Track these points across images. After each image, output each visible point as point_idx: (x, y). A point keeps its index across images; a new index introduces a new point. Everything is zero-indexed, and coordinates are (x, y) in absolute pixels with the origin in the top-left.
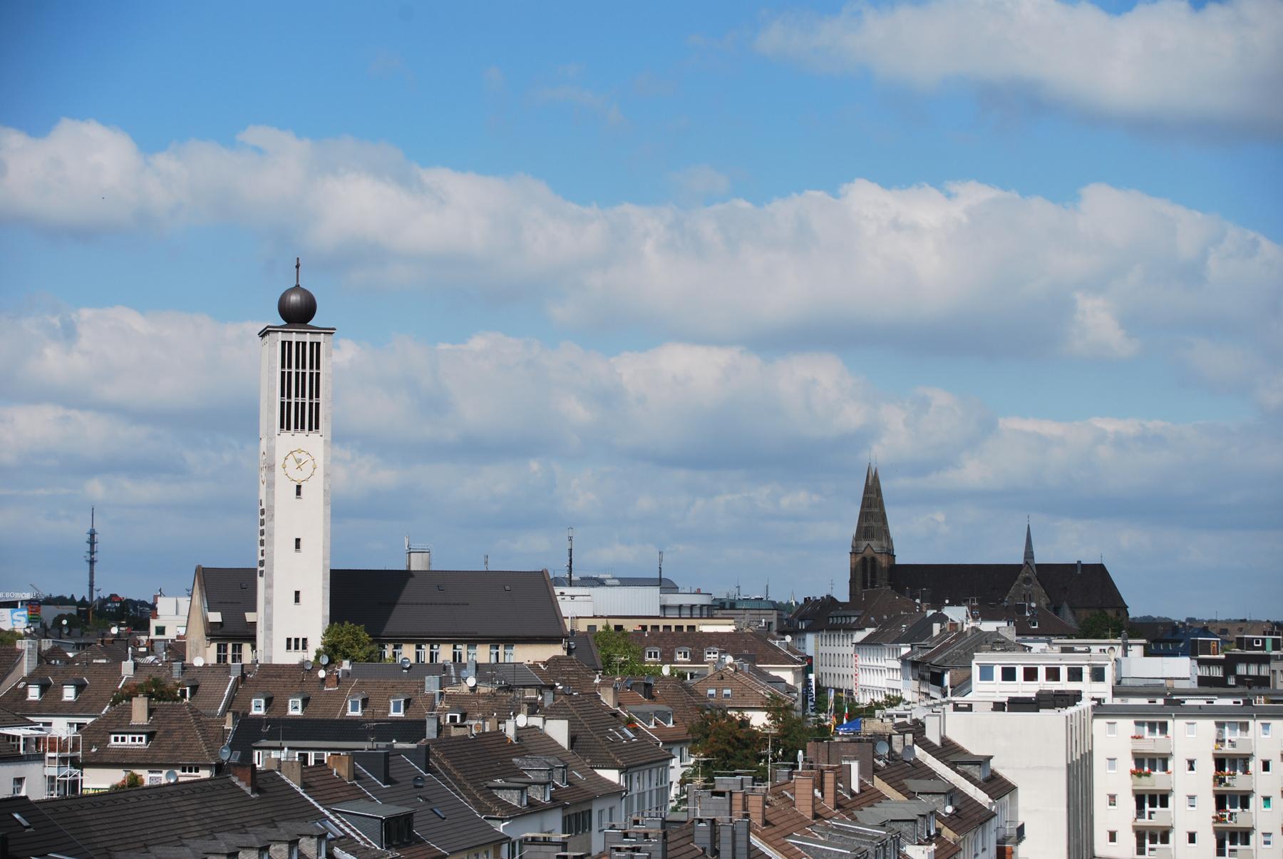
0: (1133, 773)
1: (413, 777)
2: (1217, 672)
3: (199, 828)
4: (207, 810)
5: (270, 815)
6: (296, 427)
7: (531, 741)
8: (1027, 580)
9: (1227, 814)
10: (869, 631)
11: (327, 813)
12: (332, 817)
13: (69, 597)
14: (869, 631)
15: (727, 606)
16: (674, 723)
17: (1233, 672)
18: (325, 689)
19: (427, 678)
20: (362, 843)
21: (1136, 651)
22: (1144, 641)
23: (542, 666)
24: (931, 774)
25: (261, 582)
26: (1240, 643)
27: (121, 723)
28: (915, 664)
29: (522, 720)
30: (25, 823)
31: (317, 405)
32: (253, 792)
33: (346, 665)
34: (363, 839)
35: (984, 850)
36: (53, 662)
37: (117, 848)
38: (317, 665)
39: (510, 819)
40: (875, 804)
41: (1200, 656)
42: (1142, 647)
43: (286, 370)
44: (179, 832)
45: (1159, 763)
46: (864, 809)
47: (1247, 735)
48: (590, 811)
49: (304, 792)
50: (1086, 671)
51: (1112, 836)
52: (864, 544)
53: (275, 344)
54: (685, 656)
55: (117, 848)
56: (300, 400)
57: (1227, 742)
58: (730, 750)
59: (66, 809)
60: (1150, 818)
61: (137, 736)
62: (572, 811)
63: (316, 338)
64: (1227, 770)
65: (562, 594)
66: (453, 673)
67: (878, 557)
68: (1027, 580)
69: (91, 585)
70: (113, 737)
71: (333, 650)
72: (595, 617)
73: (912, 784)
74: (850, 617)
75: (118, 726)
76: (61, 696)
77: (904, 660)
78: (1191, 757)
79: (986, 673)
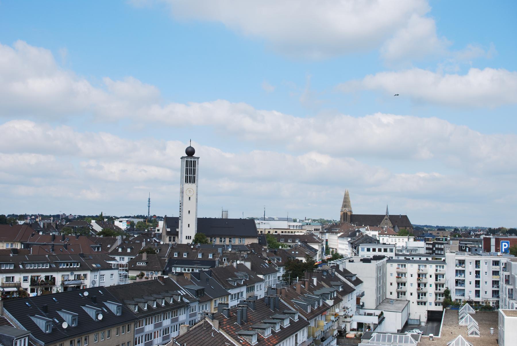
0: (397, 277)
1: (206, 278)
2: (431, 246)
3: (147, 293)
4: (150, 288)
5: (167, 289)
6: (189, 182)
7: (241, 267)
8: (386, 219)
9: (421, 289)
10: (341, 233)
11: (182, 288)
12: (183, 289)
13: (143, 215)
14: (341, 233)
15: (308, 224)
16: (281, 261)
17: (435, 246)
18: (193, 251)
19: (218, 249)
20: (191, 296)
21: (412, 239)
22: (414, 237)
23: (249, 246)
24: (339, 279)
25: (180, 221)
26: (437, 239)
27: (140, 259)
28: (352, 244)
29: (238, 262)
30: (102, 293)
31: (195, 177)
32: (163, 283)
33: (199, 245)
34: (191, 295)
35: (352, 299)
36: (126, 242)
37: (125, 299)
38: (192, 245)
39: (231, 289)
40: (321, 289)
41: (427, 242)
42: (413, 239)
43: (187, 168)
44: (142, 294)
45: (404, 275)
46: (317, 290)
47: (426, 268)
48: (254, 286)
49: (177, 283)
50: (388, 250)
51: (391, 293)
52: (344, 209)
53: (184, 161)
54: (291, 241)
55: (125, 299)
56: (190, 175)
57: (421, 270)
58: (295, 269)
59: (113, 289)
60: (401, 289)
61: (143, 263)
62: (249, 286)
63: (195, 160)
64: (421, 277)
65: (262, 223)
66: (226, 247)
67: (347, 212)
68: (386, 219)
69: (149, 212)
70: (137, 263)
71: (196, 241)
72: (270, 229)
73: (332, 283)
74: (337, 230)
75: (139, 260)
76: (127, 251)
77: (349, 242)
78: (412, 274)
79: (363, 250)
